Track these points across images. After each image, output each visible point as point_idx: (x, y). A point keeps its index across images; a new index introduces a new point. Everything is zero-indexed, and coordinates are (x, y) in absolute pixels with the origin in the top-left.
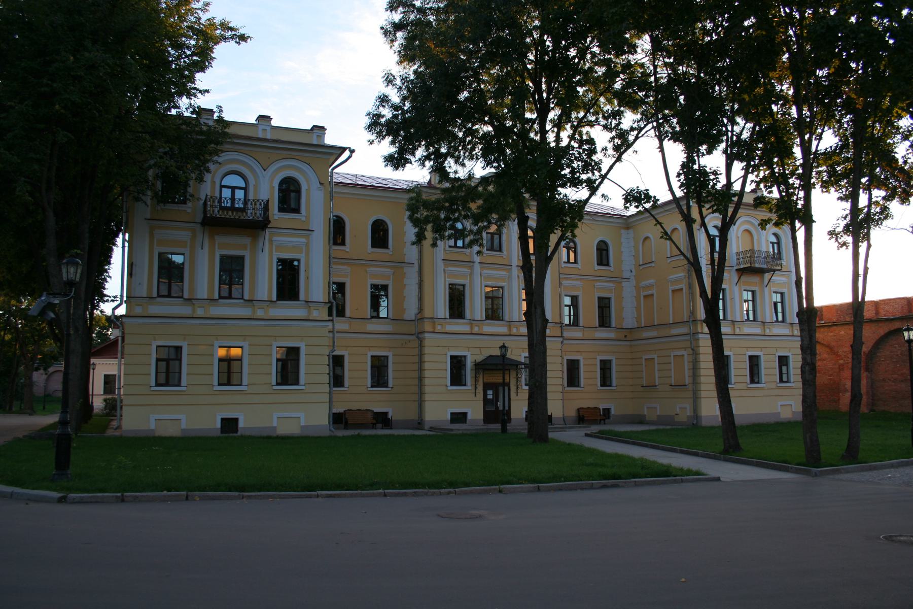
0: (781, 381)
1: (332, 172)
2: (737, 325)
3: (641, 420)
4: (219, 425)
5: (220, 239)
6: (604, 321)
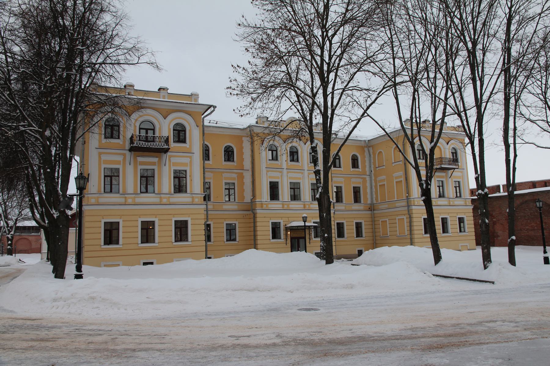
0: (460, 231)
1: (203, 120)
6: (357, 200)
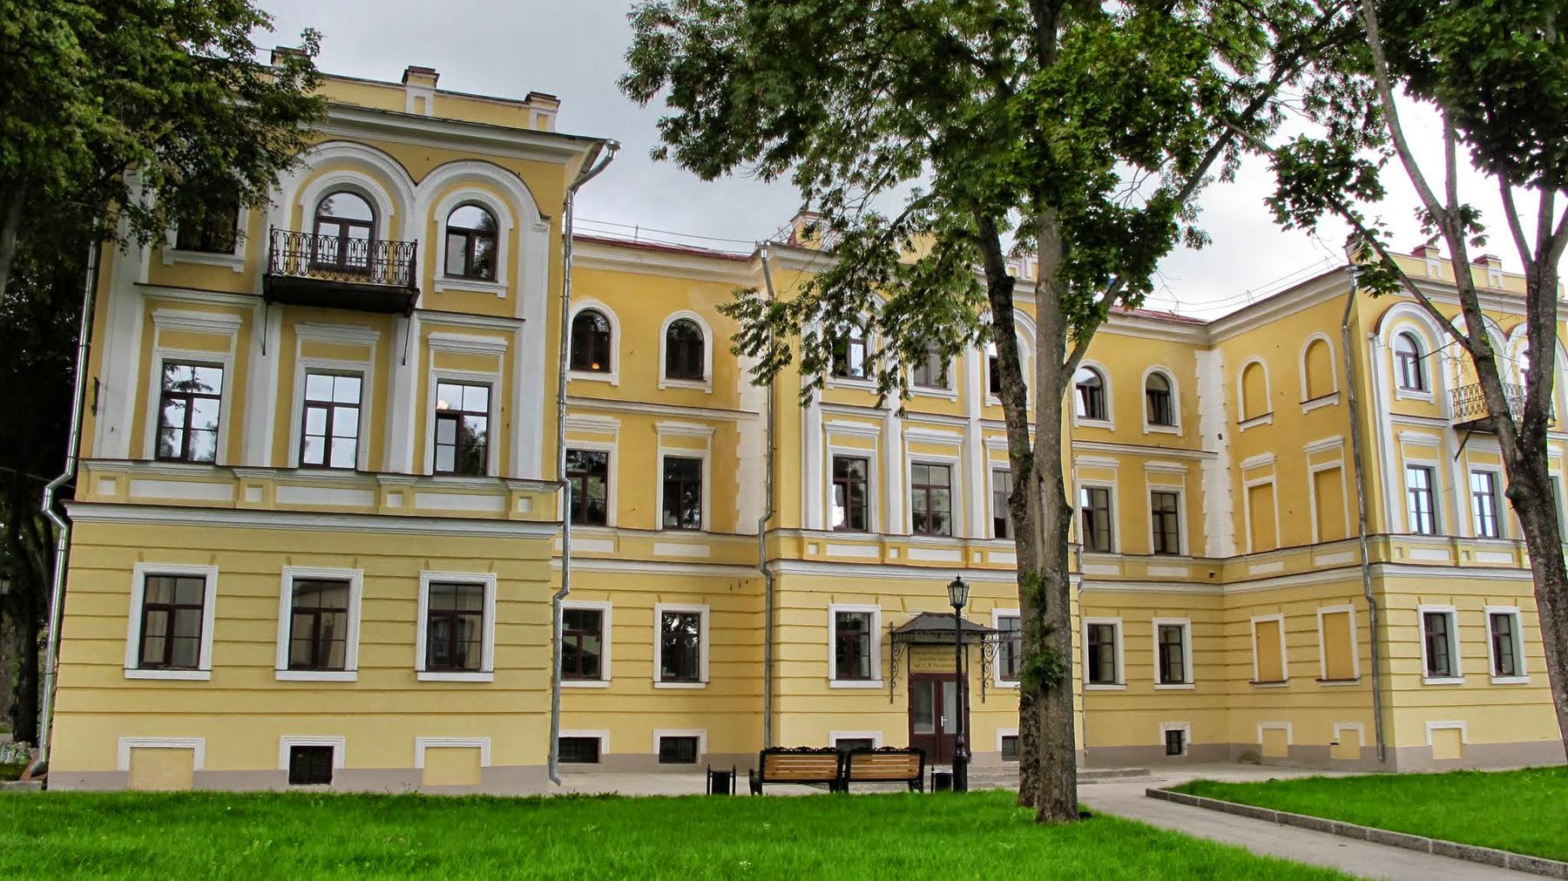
3: (1250, 756)
4: (285, 764)
6: (1165, 545)
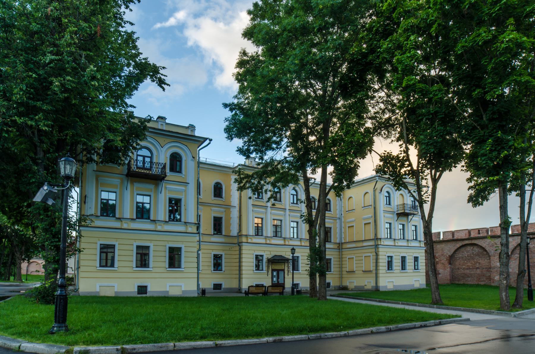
0: (415, 269)
1: (199, 152)
2: (396, 241)
5: (136, 185)
